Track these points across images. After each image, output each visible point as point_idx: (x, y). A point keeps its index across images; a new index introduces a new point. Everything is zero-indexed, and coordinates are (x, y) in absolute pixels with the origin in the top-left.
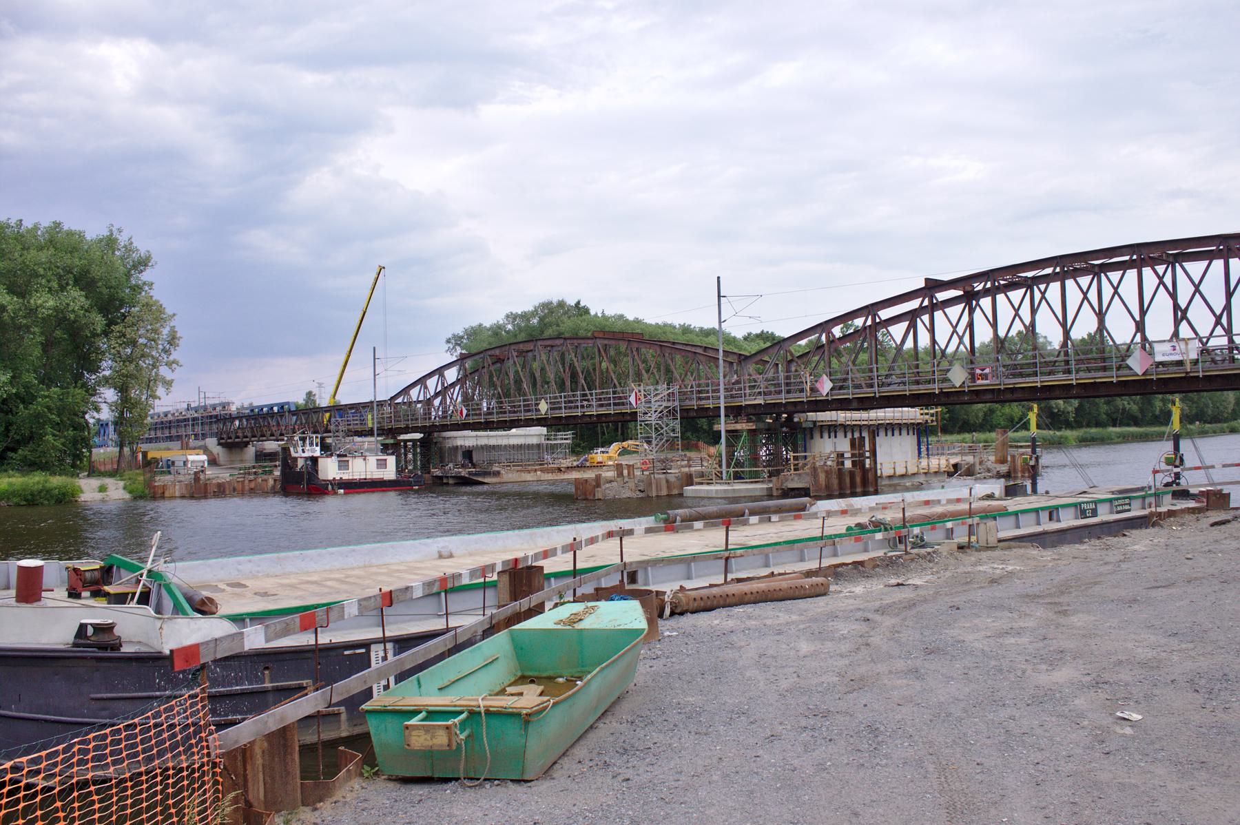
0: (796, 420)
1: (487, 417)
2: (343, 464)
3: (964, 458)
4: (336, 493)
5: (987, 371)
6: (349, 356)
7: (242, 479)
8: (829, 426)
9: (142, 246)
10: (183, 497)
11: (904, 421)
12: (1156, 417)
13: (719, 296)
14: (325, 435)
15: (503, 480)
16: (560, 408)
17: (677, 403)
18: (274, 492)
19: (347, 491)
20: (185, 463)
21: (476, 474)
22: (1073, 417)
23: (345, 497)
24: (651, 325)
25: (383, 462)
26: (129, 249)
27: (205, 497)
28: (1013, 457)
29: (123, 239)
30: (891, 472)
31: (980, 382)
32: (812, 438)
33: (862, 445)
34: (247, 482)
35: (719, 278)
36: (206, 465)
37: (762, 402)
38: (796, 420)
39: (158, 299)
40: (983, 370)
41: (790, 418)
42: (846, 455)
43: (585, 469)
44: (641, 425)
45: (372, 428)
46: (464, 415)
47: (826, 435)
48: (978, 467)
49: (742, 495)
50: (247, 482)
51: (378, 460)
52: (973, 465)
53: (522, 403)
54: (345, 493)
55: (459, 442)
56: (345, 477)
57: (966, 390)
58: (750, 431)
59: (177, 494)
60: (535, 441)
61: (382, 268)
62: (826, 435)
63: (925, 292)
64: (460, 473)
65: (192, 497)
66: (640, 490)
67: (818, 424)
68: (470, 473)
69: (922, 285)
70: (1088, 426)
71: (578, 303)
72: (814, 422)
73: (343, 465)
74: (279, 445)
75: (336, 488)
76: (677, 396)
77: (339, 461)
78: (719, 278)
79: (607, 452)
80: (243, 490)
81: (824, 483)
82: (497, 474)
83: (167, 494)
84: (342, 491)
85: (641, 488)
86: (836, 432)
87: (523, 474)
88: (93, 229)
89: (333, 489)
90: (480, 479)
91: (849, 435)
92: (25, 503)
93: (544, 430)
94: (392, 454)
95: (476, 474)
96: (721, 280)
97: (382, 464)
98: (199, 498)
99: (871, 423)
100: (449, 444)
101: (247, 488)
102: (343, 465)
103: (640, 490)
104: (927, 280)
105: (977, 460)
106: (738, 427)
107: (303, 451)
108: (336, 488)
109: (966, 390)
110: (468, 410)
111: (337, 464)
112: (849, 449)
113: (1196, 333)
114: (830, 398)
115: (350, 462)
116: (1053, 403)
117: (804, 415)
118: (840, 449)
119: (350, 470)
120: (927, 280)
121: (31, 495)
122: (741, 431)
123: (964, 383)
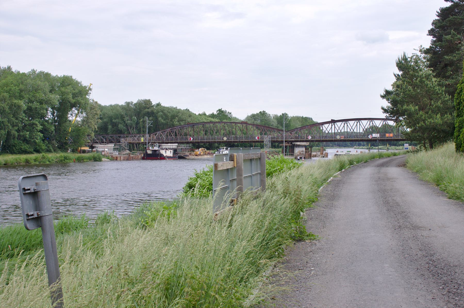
5: (343, 137)
16: (204, 140)
58: (289, 146)
68: (184, 155)
90: (186, 157)
93: (177, 144)
106: (287, 145)
110: (193, 138)
122: (287, 146)
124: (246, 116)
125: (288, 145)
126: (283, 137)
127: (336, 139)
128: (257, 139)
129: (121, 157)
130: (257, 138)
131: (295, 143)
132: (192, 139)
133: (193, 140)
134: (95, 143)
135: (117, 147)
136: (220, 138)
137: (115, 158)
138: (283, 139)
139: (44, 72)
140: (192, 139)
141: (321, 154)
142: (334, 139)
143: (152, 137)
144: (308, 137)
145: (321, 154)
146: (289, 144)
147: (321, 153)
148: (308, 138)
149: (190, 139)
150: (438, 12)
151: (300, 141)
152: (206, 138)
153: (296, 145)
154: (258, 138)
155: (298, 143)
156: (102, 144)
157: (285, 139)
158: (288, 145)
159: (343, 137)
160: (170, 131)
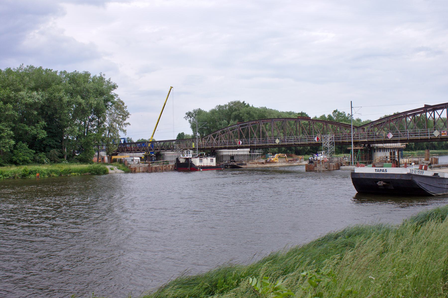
0: (371, 146)
1: (251, 144)
3: (413, 159)
4: (200, 170)
5: (445, 132)
6: (159, 121)
7: (162, 166)
9: (114, 81)
10: (143, 172)
11: (397, 147)
12: (442, 146)
13: (352, 107)
14: (117, 152)
15: (247, 167)
16: (267, 143)
17: (334, 141)
18: (172, 170)
20: (133, 160)
21: (240, 164)
22: (414, 147)
23: (203, 171)
24: (257, 109)
25: (212, 160)
26: (109, 82)
27: (152, 172)
28: (432, 159)
29: (107, 79)
31: (443, 135)
32: (375, 152)
33: (394, 154)
34: (164, 167)
35: (351, 101)
36: (140, 160)
37: (367, 141)
38: (371, 146)
40: (444, 132)
41: (369, 146)
42: (388, 157)
43: (271, 163)
44: (324, 147)
46: (241, 144)
47: (382, 151)
48: (419, 162)
50: (164, 167)
51: (211, 159)
52: (418, 161)
53: (307, 140)
54: (202, 170)
55: (224, 154)
57: (439, 138)
58: (361, 150)
59: (141, 171)
60: (246, 153)
61: (172, 87)
62: (382, 151)
63: (424, 108)
64: (233, 164)
65: (147, 172)
66: (326, 168)
68: (237, 164)
69: (424, 106)
70: (419, 150)
71: (244, 102)
72: (377, 147)
73: (201, 161)
74: (143, 155)
75: (200, 168)
76: (334, 138)
78: (351, 101)
79: (274, 157)
80: (162, 170)
82: (245, 164)
83: (137, 171)
84: (202, 170)
85: (327, 167)
86: (381, 150)
87: (253, 165)
88: (94, 72)
90: (240, 166)
91: (390, 151)
92: (96, 173)
93: (249, 150)
94: (215, 157)
95: (240, 164)
96: (352, 102)
97: (212, 161)
98: (150, 172)
99: (391, 147)
100: (222, 154)
101: (164, 169)
102: (201, 161)
103: (326, 168)
104: (425, 105)
105: (419, 160)
106: (357, 148)
107: (187, 156)
109: (439, 138)
110: (242, 142)
111: (199, 161)
112: (389, 155)
113: (441, 115)
114: (392, 140)
115: (203, 160)
116: (434, 142)
117: (374, 144)
118: (387, 155)
119: (203, 163)
120: (425, 105)
121: (98, 170)
122: (358, 149)
123: (439, 135)
124: (290, 111)
125: (359, 148)
126: (351, 137)
127: (432, 136)
128: (316, 140)
129: (141, 168)
130: (316, 139)
131: (374, 145)
132: (241, 143)
133: (242, 144)
134: (168, 149)
135: (352, 139)
136: (284, 140)
137: (134, 170)
138: (351, 139)
139: (52, 70)
140: (241, 143)
141: (425, 160)
142: (429, 137)
143: (203, 142)
144: (388, 136)
145: (425, 160)
146: (360, 146)
147: (426, 158)
148: (387, 137)
149: (239, 143)
150: (114, 87)
151: (381, 142)
152: (269, 141)
153: (375, 148)
154: (318, 139)
155: (380, 145)
156: (167, 150)
157: (354, 139)
158: (359, 148)
159: (445, 132)
160: (240, 128)
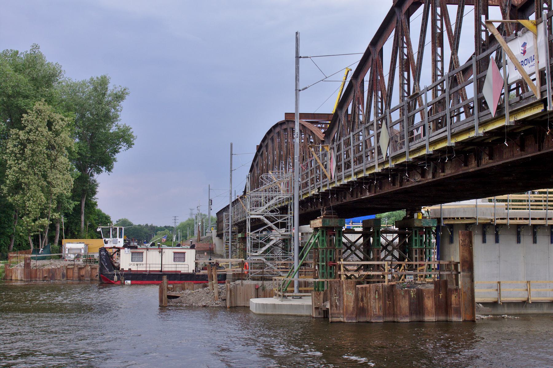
2: (136, 256)
7: (73, 267)
8: (467, 226)
19: (134, 282)
25: (182, 256)
30: (490, 299)
35: (231, 145)
39: (117, 159)
45: (208, 219)
49: (285, 313)
51: (175, 253)
54: (132, 284)
56: (142, 268)
67: (443, 223)
75: (122, 279)
77: (132, 253)
78: (231, 145)
81: (352, 304)
84: (129, 282)
89: (119, 279)
97: (179, 257)
108: (122, 279)
111: (130, 255)
115: (144, 254)
119: (144, 262)
